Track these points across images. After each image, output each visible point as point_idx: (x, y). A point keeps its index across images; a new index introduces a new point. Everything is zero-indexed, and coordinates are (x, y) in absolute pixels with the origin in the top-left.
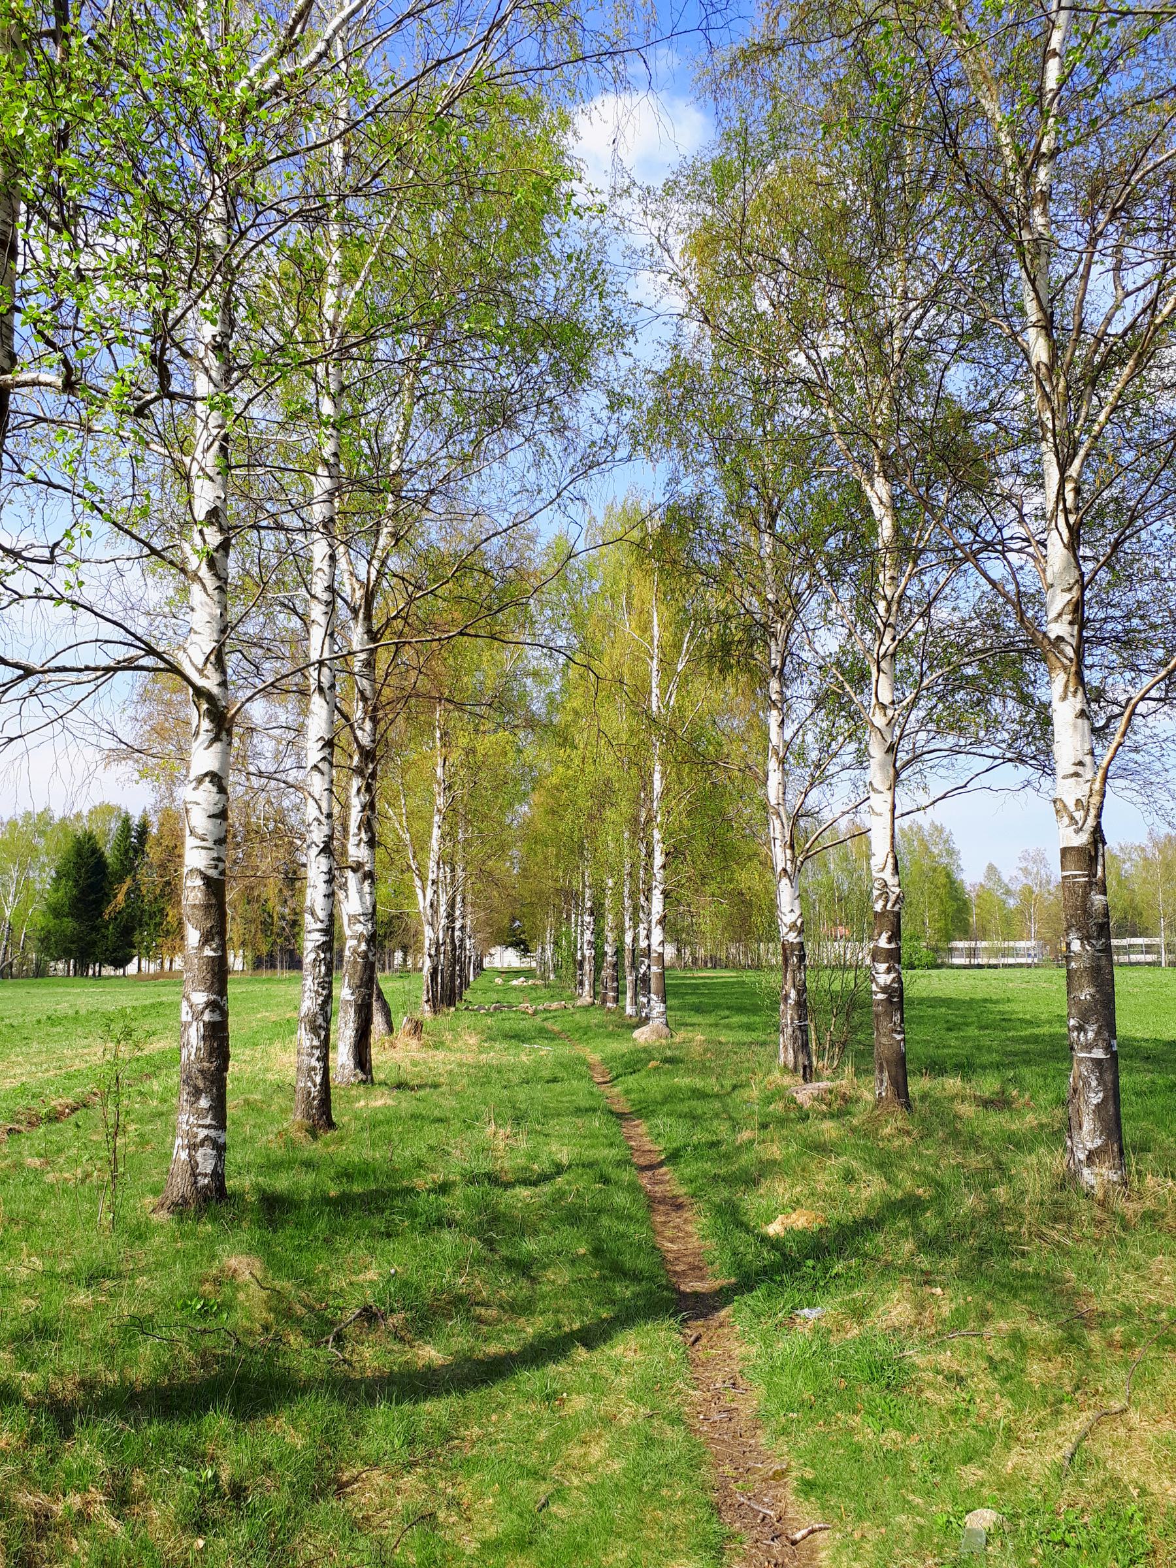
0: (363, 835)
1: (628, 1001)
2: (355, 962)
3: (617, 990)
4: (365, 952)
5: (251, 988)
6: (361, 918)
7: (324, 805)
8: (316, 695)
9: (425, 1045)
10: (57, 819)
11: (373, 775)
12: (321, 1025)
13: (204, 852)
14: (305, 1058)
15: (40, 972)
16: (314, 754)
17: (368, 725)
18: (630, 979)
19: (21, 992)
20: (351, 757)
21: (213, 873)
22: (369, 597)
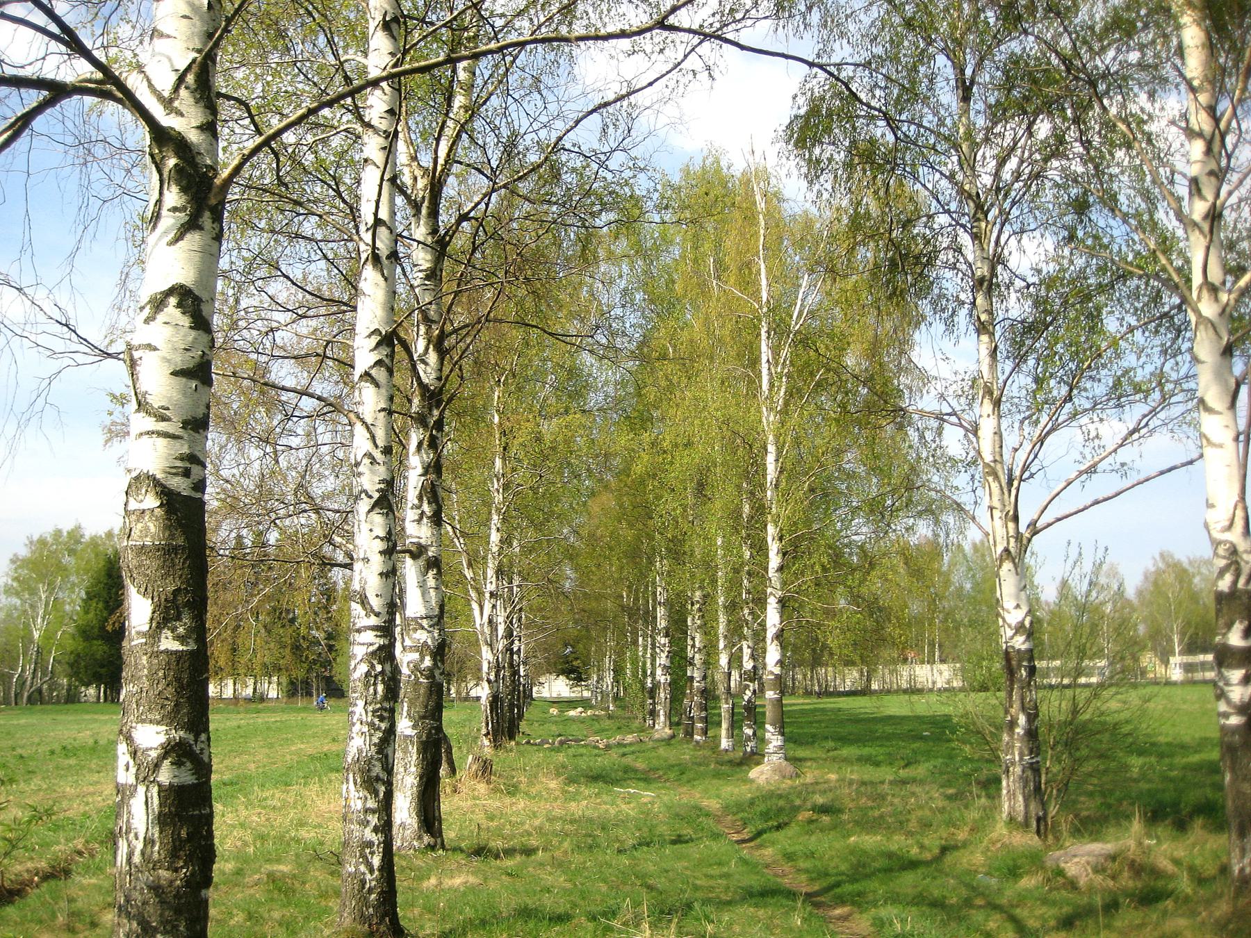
0: (426, 507)
1: (724, 733)
2: (417, 682)
3: (705, 720)
4: (431, 670)
5: (285, 717)
6: (425, 623)
7: (380, 434)
8: (369, 267)
9: (496, 790)
10: (87, 537)
11: (439, 425)
12: (378, 779)
13: (162, 442)
14: (355, 827)
15: (72, 698)
16: (365, 356)
17: (432, 357)
18: (725, 707)
19: (47, 719)
20: (410, 401)
21: (179, 484)
22: (436, 187)
